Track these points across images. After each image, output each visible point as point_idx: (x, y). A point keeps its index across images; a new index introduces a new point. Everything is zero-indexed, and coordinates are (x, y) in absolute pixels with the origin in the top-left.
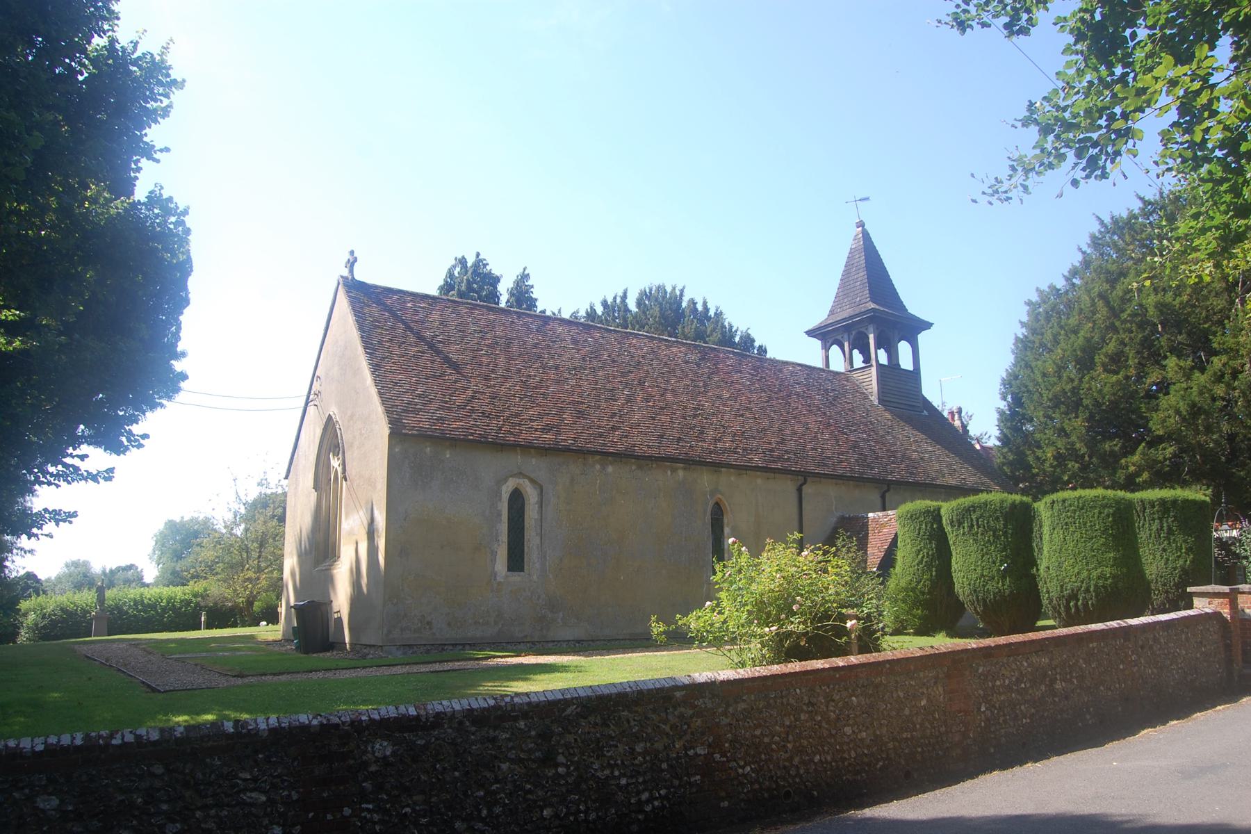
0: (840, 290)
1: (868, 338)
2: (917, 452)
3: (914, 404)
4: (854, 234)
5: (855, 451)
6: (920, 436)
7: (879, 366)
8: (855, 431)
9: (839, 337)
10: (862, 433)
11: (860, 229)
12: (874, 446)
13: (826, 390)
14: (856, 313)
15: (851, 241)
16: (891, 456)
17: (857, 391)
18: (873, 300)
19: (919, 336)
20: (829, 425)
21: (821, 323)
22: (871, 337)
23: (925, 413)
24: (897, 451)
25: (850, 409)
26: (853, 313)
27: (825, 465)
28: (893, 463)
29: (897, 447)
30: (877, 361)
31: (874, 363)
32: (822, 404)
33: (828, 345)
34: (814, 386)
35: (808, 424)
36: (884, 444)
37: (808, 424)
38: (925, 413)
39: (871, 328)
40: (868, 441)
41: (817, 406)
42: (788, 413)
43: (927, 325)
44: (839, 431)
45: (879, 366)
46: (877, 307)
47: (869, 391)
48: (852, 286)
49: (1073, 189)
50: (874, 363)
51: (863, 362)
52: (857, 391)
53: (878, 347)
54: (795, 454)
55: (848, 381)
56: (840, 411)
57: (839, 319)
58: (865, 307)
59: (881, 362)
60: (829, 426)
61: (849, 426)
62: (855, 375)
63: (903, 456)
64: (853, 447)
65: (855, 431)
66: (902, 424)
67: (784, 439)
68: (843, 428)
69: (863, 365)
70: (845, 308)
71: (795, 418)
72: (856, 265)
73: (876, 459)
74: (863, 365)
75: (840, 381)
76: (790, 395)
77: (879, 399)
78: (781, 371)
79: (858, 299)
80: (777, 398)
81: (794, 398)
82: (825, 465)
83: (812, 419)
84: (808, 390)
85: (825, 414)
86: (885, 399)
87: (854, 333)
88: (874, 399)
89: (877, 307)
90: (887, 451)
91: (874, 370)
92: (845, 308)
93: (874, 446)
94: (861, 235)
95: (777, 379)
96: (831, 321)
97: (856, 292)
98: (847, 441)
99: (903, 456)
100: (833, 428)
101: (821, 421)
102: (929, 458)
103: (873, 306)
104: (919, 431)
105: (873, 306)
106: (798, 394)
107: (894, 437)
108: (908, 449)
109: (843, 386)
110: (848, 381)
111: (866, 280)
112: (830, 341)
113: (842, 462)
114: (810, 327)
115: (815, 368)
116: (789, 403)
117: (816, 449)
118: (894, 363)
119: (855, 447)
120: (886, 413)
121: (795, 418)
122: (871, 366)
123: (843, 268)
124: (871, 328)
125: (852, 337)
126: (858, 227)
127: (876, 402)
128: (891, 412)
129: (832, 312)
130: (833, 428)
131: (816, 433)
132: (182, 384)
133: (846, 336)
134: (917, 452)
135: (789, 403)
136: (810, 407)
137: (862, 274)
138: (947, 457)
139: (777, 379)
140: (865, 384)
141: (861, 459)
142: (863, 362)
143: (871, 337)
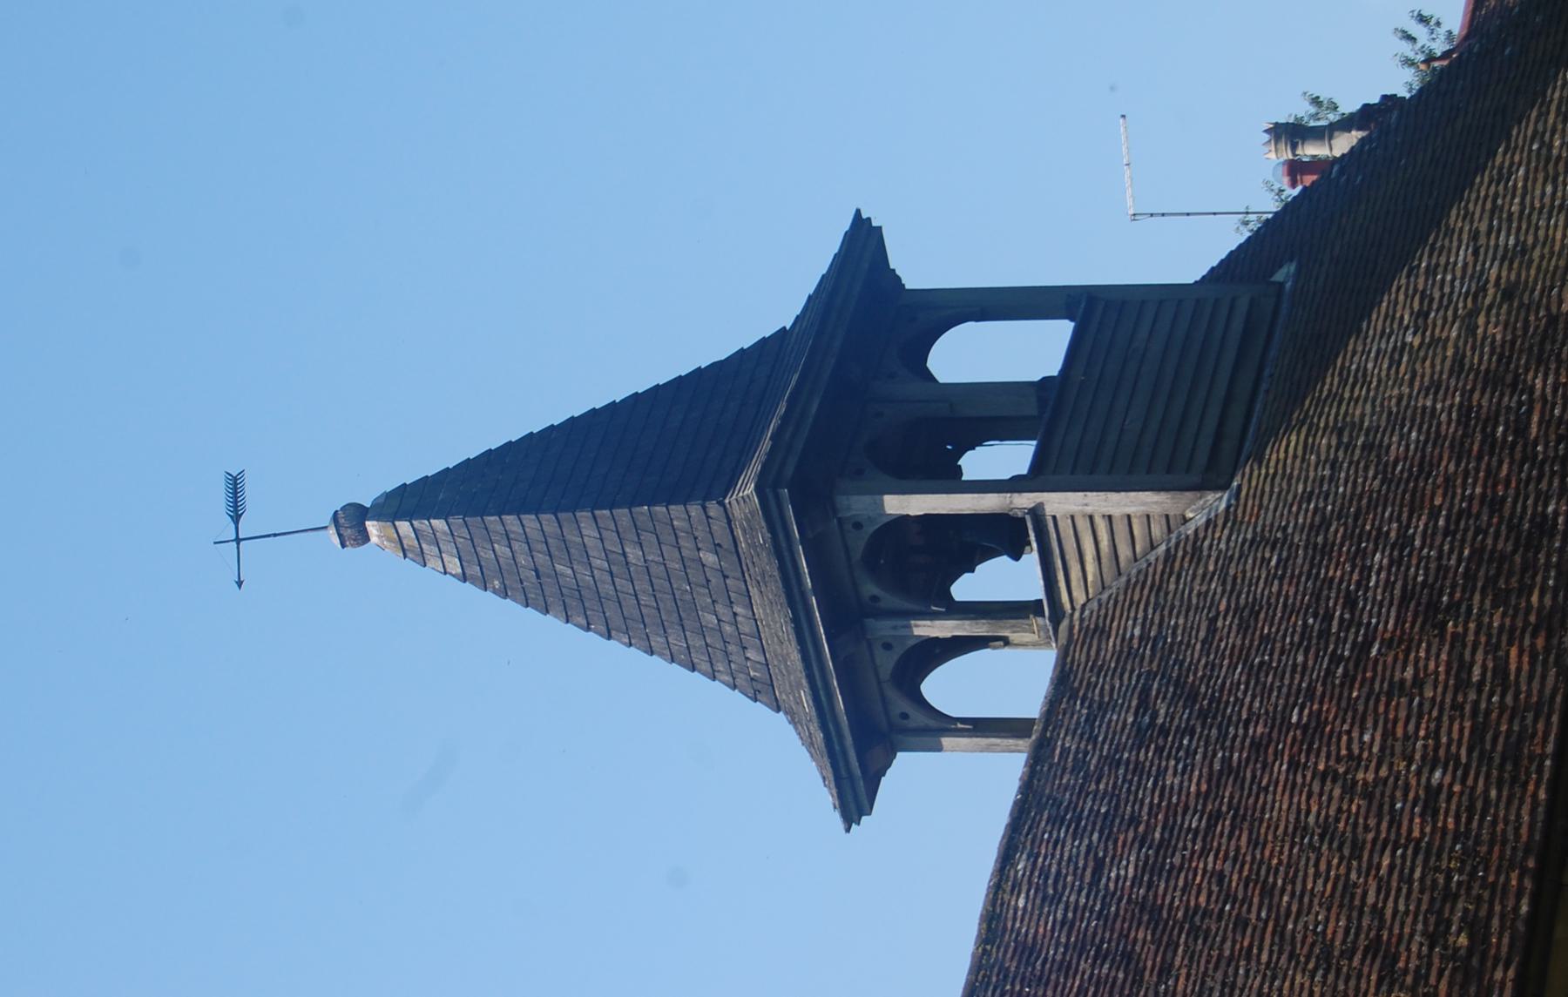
0: (657, 641)
1: (903, 522)
2: (1473, 314)
3: (1237, 325)
4: (393, 556)
5: (1453, 606)
6: (1400, 301)
7: (1038, 477)
8: (1350, 602)
9: (886, 662)
10: (1366, 571)
11: (372, 527)
12: (1434, 514)
13: (1141, 737)
14: (772, 568)
15: (429, 576)
16: (1489, 441)
17: (1158, 588)
18: (718, 486)
19: (910, 282)
20: (1314, 729)
21: (809, 744)
22: (898, 505)
23: (1285, 274)
24: (1466, 410)
25: (1244, 628)
26: (775, 587)
27: (1513, 755)
28: (1521, 429)
29: (1446, 409)
30: (1015, 485)
31: (1023, 501)
32: (1209, 758)
33: (918, 718)
34: (1113, 796)
35: (1301, 828)
36: (1425, 467)
37: (1301, 828)
38: (1285, 274)
39: (855, 505)
40: (1404, 541)
41: (1215, 782)
42: (1241, 924)
43: (858, 212)
44: (1348, 679)
45: (1038, 477)
46: (755, 467)
47: (1157, 531)
48: (642, 585)
49: (860, 207)
50: (1023, 501)
51: (1016, 556)
52: (1158, 588)
53: (950, 479)
54: (1450, 896)
55: (1101, 632)
56: (1250, 670)
57: (795, 656)
58: (750, 531)
59: (1023, 468)
60: (1320, 725)
61: (1324, 634)
62: (1076, 595)
63: (1491, 380)
64: (1434, 619)
65: (1350, 602)
66: (1331, 381)
67: (1373, 948)
68: (1336, 659)
69: (1031, 559)
70: (746, 627)
71: (1267, 891)
72: (541, 558)
73: (1496, 505)
74: (1031, 559)
75: (1098, 669)
76: (1150, 912)
77: (1202, 487)
78: (1027, 951)
79: (709, 558)
80: (1165, 971)
81: (1171, 896)
82: (1513, 755)
83: (1280, 807)
84: (1134, 820)
85: (1258, 746)
86: (1202, 457)
87: (870, 589)
88: (1200, 508)
89: (755, 467)
90: (1460, 452)
91: (1058, 504)
92: (746, 627)
93: (1434, 514)
94: (404, 527)
95: (1066, 968)
96: (805, 696)
97: (675, 566)
98: (1401, 643)
99: (1491, 380)
100: (1330, 709)
101: (1294, 765)
102: (1507, 257)
103: (747, 489)
104: (1375, 303)
105: (747, 489)
106: (1151, 870)
107: (1395, 421)
108: (1459, 360)
109: (1127, 653)
110: (1101, 632)
111: (622, 513)
112: (900, 704)
113: (1501, 671)
114: (822, 799)
115: (1029, 787)
116: (1190, 914)
117: (1433, 793)
118: (1031, 409)
119: (1433, 606)
120: (1273, 455)
121: (1267, 891)
122: (1037, 513)
123: (551, 624)
124: (855, 505)
125: (890, 601)
126: (366, 539)
127: (1217, 501)
128: (1271, 433)
129: (762, 690)
130: (1330, 709)
131: (1349, 789)
132: (864, 216)
133: (883, 628)
134: (1473, 314)
135: (1190, 914)
136: (1215, 817)
137: (590, 531)
138: (1503, 176)
139: (1066, 968)
140: (1124, 552)
141: (1491, 581)
142: (1016, 556)
143: (898, 505)
